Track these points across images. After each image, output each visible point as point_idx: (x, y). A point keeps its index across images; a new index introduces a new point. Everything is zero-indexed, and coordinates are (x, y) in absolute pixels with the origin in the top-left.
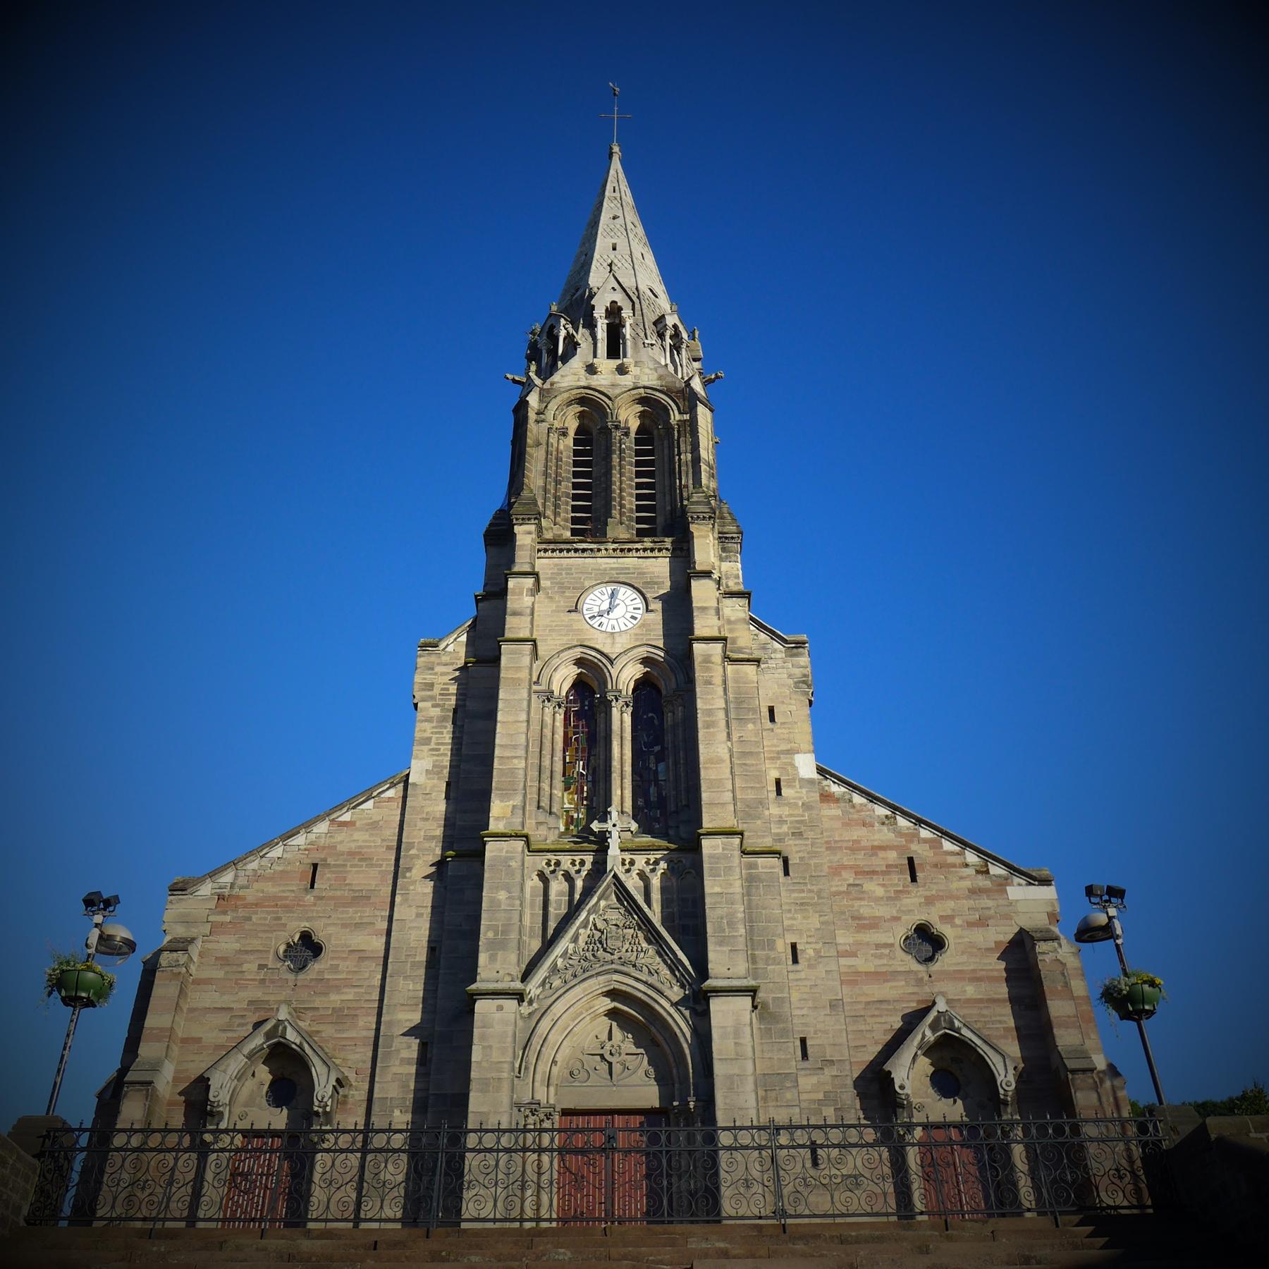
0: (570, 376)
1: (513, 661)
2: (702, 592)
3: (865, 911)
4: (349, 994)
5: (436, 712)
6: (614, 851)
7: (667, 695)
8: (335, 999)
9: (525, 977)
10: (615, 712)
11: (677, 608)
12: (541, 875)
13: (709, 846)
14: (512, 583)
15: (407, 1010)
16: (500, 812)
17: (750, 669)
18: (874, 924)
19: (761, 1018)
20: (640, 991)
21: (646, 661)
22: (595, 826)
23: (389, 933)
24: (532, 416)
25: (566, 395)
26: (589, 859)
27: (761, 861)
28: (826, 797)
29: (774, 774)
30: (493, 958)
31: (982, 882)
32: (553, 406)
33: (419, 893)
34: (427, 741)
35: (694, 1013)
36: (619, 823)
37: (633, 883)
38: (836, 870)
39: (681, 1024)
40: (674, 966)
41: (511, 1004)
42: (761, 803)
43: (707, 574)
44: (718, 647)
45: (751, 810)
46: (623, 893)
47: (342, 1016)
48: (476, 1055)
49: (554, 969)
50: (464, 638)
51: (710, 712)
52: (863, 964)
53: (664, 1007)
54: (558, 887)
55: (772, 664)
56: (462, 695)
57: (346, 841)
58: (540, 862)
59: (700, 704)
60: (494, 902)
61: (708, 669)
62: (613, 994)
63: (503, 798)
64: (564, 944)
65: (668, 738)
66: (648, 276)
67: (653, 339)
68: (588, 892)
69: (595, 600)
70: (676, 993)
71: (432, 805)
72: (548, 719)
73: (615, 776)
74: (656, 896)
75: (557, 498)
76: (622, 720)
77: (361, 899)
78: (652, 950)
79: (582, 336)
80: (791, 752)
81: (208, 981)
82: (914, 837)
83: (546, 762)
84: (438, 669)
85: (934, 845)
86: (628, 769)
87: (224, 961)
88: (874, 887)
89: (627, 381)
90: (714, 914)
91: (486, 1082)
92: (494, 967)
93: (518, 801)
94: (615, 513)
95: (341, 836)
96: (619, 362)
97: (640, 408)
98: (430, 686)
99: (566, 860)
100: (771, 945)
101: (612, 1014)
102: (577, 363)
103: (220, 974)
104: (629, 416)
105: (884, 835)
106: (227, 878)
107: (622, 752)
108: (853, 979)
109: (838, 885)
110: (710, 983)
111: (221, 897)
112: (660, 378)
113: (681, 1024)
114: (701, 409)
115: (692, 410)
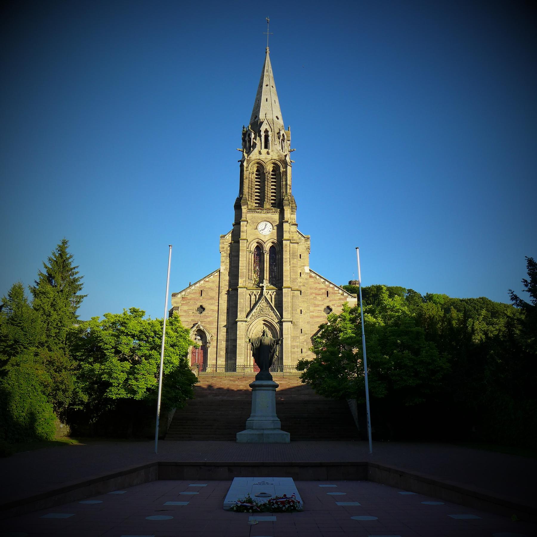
0: (254, 155)
1: (243, 245)
2: (286, 226)
3: (316, 303)
4: (211, 319)
5: (225, 254)
6: (265, 290)
7: (277, 250)
8: (209, 319)
9: (247, 317)
10: (265, 256)
11: (280, 229)
12: (250, 295)
13: (284, 290)
14: (242, 223)
15: (223, 322)
16: (241, 282)
17: (296, 245)
18: (318, 306)
19: (293, 325)
20: (269, 320)
21: (273, 243)
22: (261, 285)
23: (218, 306)
24: (245, 169)
25: (253, 162)
26: (259, 291)
27: (295, 292)
28: (311, 277)
29: (300, 271)
30: (240, 314)
31: (342, 297)
32: (250, 165)
33: (224, 298)
34: (223, 262)
35: (280, 325)
36: (266, 283)
37: (268, 297)
38: (311, 294)
39: (277, 327)
40: (276, 315)
41: (244, 323)
42: (296, 278)
43: (287, 222)
44: (289, 242)
45: (294, 280)
46: (266, 300)
47: (210, 323)
48: (238, 333)
49: (253, 315)
50: (230, 235)
51: (286, 259)
52: (315, 314)
53: (274, 324)
54: (253, 297)
55: (301, 243)
56: (231, 250)
57: (208, 285)
58: (249, 292)
59: (284, 257)
60: (240, 302)
61: (286, 248)
62: (264, 320)
63: (242, 278)
64: (254, 310)
65: (277, 261)
66: (277, 112)
67: (277, 140)
68: (259, 299)
69: (261, 226)
70: (277, 321)
71: (226, 278)
72: (249, 353)
73: (265, 272)
74: (273, 300)
75: (251, 194)
76: (267, 257)
77: (212, 298)
78: (272, 312)
79: (258, 142)
80: (304, 266)
81: (182, 316)
82: (328, 286)
83: (250, 268)
84: (225, 243)
85: (333, 288)
86: (268, 269)
87: (185, 311)
88: (319, 298)
89: (269, 157)
90: (285, 305)
91: (240, 338)
92: (241, 315)
93: (244, 279)
94: (266, 200)
95: (206, 284)
96: (267, 150)
97: (273, 165)
98: (223, 248)
99: (255, 291)
100: (296, 310)
101: (264, 324)
102: (256, 151)
103: (185, 314)
104: (269, 168)
105: (323, 286)
106: (183, 293)
107: (267, 265)
108: (312, 317)
109: (312, 297)
110: (283, 320)
111: (183, 298)
112: (278, 156)
113: (277, 327)
114: (289, 168)
115: (286, 167)
